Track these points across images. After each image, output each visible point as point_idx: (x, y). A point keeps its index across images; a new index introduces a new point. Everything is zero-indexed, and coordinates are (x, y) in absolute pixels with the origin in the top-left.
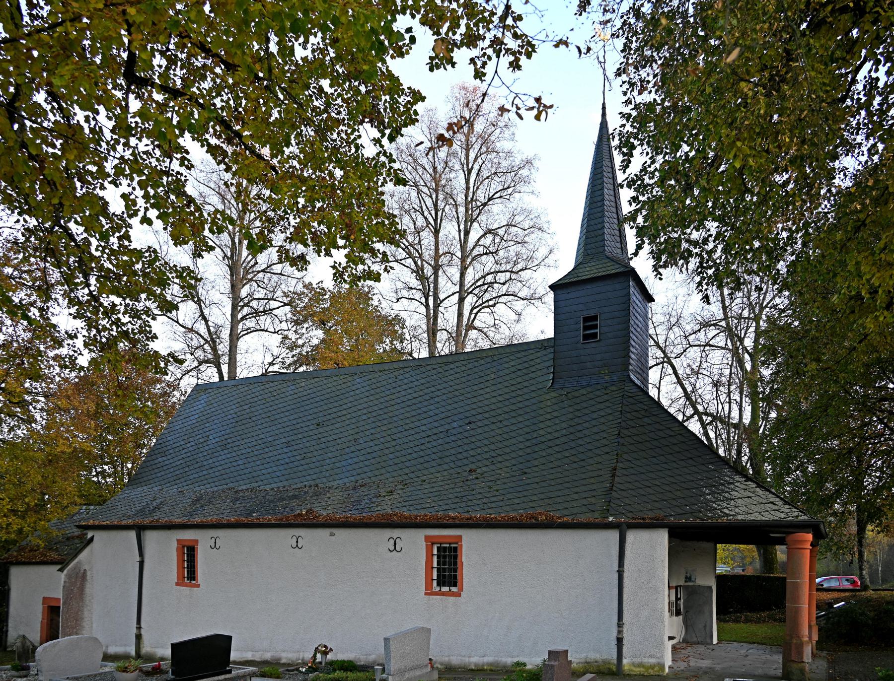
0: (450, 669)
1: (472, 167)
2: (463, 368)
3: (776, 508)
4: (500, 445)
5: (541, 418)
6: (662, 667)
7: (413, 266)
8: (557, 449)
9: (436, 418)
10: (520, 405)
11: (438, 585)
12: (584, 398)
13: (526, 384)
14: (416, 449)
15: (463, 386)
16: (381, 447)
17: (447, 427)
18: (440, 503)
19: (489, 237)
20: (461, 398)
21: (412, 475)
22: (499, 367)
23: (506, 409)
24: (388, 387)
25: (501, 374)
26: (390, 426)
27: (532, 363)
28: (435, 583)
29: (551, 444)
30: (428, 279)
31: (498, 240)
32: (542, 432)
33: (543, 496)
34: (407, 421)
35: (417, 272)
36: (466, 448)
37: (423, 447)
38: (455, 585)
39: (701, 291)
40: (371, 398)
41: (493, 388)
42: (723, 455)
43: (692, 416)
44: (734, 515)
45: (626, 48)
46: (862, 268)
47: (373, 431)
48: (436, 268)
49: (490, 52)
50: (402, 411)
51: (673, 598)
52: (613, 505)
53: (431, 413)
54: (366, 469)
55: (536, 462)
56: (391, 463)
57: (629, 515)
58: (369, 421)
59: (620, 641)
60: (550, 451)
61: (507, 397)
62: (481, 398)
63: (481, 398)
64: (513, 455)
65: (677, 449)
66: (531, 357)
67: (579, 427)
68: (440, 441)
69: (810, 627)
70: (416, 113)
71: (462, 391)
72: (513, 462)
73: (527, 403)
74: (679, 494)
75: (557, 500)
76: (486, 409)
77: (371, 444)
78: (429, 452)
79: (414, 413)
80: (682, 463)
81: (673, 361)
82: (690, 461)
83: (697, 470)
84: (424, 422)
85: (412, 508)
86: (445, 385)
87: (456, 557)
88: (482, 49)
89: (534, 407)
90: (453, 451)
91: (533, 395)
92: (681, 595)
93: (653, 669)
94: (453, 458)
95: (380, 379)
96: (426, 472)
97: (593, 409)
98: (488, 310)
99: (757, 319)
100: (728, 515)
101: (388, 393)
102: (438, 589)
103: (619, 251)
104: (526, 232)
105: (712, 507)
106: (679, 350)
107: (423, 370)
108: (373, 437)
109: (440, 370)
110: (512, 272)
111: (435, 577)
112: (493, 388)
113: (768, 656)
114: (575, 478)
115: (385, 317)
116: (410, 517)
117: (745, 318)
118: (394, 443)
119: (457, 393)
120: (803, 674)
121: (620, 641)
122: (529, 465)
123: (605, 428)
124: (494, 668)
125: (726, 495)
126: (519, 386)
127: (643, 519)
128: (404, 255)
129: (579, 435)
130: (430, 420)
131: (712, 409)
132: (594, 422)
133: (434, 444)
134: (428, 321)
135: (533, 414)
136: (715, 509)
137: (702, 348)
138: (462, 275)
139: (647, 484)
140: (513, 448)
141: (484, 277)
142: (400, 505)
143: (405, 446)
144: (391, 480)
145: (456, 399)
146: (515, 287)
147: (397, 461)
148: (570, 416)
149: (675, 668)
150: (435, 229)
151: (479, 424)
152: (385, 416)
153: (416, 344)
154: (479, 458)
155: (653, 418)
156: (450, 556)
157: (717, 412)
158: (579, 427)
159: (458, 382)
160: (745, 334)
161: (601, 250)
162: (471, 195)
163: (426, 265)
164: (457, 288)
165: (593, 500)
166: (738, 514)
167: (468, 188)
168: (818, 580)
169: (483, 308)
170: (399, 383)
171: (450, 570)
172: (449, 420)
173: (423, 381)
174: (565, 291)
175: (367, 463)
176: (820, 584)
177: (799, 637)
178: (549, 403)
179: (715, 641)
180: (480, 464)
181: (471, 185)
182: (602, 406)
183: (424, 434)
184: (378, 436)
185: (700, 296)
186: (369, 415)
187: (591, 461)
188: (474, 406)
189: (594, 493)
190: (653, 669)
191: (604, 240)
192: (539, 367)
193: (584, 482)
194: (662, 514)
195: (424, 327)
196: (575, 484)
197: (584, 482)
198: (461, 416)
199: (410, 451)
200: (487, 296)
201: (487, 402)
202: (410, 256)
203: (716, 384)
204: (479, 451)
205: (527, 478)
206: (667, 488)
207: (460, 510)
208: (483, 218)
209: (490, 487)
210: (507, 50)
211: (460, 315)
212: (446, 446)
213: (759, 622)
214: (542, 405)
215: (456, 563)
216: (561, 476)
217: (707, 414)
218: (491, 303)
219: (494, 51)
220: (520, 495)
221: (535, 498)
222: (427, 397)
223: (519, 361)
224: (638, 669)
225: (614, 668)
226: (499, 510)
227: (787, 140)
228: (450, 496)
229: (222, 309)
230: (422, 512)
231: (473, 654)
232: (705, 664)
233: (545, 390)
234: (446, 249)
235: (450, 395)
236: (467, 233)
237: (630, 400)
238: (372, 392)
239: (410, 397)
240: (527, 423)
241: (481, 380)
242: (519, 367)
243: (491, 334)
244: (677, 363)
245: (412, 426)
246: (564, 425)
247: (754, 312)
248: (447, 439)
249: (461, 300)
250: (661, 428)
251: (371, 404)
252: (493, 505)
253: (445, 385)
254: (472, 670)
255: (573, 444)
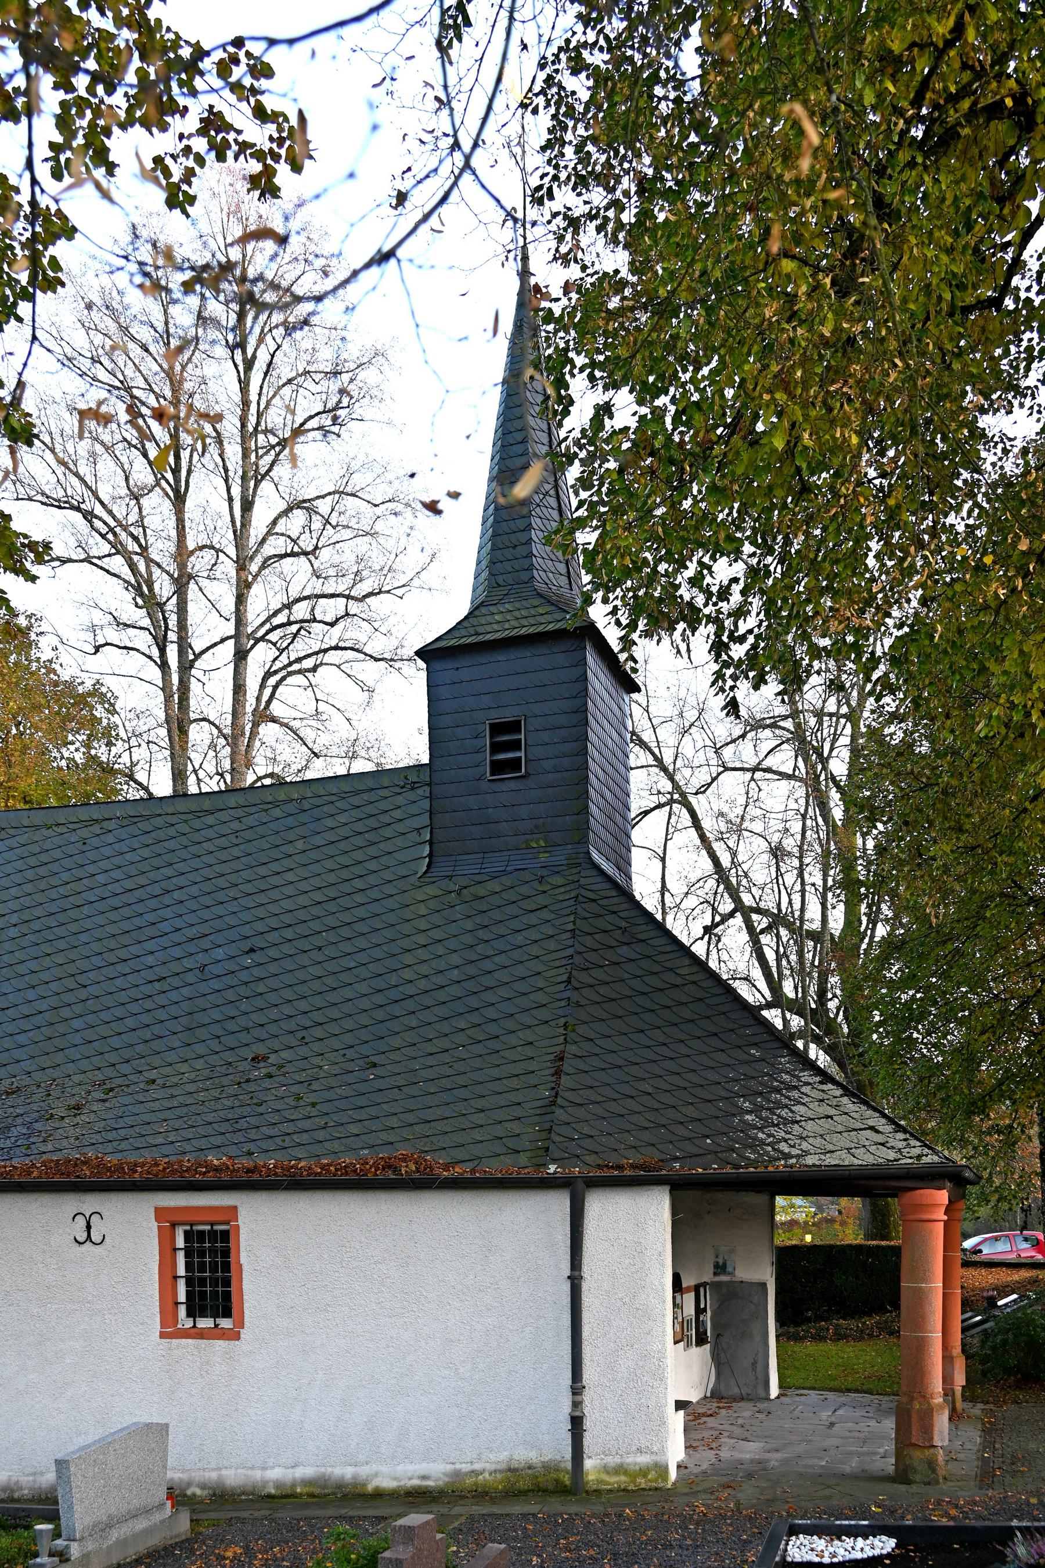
0: (222, 1496)
1: (254, 357)
2: (236, 825)
3: (880, 1138)
4: (318, 1001)
5: (406, 943)
6: (663, 1470)
7: (126, 572)
8: (442, 1011)
9: (176, 937)
10: (361, 912)
11: (190, 1314)
12: (496, 900)
13: (372, 865)
14: (134, 1008)
15: (236, 865)
16: (54, 1002)
17: (202, 959)
18: (189, 1134)
19: (299, 517)
20: (232, 893)
21: (125, 1069)
22: (314, 826)
23: (331, 921)
24: (67, 863)
25: (318, 840)
26: (73, 955)
27: (386, 819)
28: (182, 1311)
29: (427, 1000)
30: (161, 606)
31: (317, 524)
32: (408, 974)
33: (410, 1118)
34: (113, 944)
35: (138, 590)
36: (244, 1006)
37: (148, 1004)
38: (227, 1313)
39: (722, 690)
40: (28, 888)
41: (303, 872)
42: (791, 995)
43: (731, 915)
44: (798, 1156)
45: (553, 143)
46: (1032, 666)
47: (33, 965)
48: (182, 582)
49: (200, 145)
50: (100, 920)
51: (689, 1310)
52: (558, 1139)
53: (166, 927)
54: (20, 1054)
55: (396, 1042)
56: (77, 1039)
57: (590, 1159)
58: (25, 942)
59: (577, 1423)
60: (426, 1016)
61: (332, 892)
62: (275, 894)
63: (275, 894)
64: (349, 1024)
65: (687, 1014)
66: (383, 805)
67: (487, 965)
68: (186, 991)
69: (948, 1359)
70: (54, 263)
71: (233, 878)
72: (348, 1039)
73: (375, 908)
74: (691, 1111)
75: (440, 1126)
76: (288, 919)
77: (31, 995)
78: (162, 1015)
79: (126, 926)
80: (696, 1044)
81: (692, 799)
82: (714, 1041)
83: (728, 1061)
84: (150, 946)
85: (124, 1145)
86: (196, 863)
87: (226, 1253)
88: (181, 137)
89: (391, 918)
90: (216, 1014)
91: (389, 890)
92: (708, 1302)
93: (645, 1476)
94: (216, 1029)
95: (48, 845)
96: (156, 1061)
97: (515, 924)
98: (299, 679)
99: (853, 717)
100: (788, 1156)
101: (65, 876)
102: (189, 1324)
103: (563, 581)
104: (378, 511)
105: (755, 1138)
106: (702, 777)
107: (144, 826)
108: (33, 979)
109: (184, 828)
110: (348, 597)
111: (182, 1297)
112: (303, 872)
113: (873, 1423)
114: (478, 1076)
115: (70, 685)
116: (119, 1168)
117: (831, 715)
118: (83, 994)
119: (222, 882)
120: (934, 1471)
121: (577, 1423)
122: (381, 1046)
123: (541, 968)
124: (317, 1491)
125: (784, 1113)
126: (358, 870)
127: (619, 1167)
128: (106, 548)
129: (487, 981)
130: (164, 941)
131: (769, 903)
132: (516, 955)
133: (174, 996)
134: (168, 699)
135: (389, 933)
136: (763, 1143)
137: (749, 775)
138: (241, 600)
139: (627, 1090)
140: (347, 1008)
141: (288, 606)
142: (96, 1138)
143: (108, 1001)
144: (76, 1078)
145: (221, 896)
146: (354, 632)
147: (90, 1034)
148: (468, 939)
149: (691, 1466)
150: (176, 491)
151: (273, 953)
152: (61, 932)
153: (140, 754)
154: (273, 1029)
155: (639, 948)
156: (213, 1252)
157: (779, 910)
158: (487, 965)
159: (224, 855)
160: (832, 749)
161: (525, 576)
162: (252, 419)
163: (156, 572)
164: (230, 629)
165: (515, 1127)
166: (807, 1153)
167: (246, 403)
168: (968, 1244)
169: (290, 674)
170: (92, 855)
171: (215, 1282)
172: (205, 943)
173: (146, 852)
174: (450, 664)
175: (21, 1039)
176: (975, 1251)
177: (925, 1397)
178: (422, 910)
179: (774, 1391)
180: (275, 1044)
181: (253, 397)
182: (533, 919)
183: (150, 975)
184: (45, 976)
185: (721, 700)
186: (24, 928)
187: (512, 1040)
188: (261, 912)
189: (517, 1112)
190: (645, 1476)
191: (531, 555)
192: (400, 827)
193: (497, 1086)
194: (658, 1156)
195: (162, 716)
196: (478, 1090)
197: (497, 1086)
198: (233, 934)
199: (119, 1012)
200: (300, 648)
201: (287, 904)
202: (119, 549)
203: (777, 853)
204: (274, 1014)
205: (377, 1077)
206: (668, 1099)
207: (233, 1151)
208: (282, 471)
209: (298, 1098)
210: (244, 146)
211: (239, 688)
212: (201, 1003)
213: (860, 1339)
214: (408, 914)
215: (227, 1267)
216: (450, 1072)
217: (758, 911)
218: (308, 663)
219: (212, 146)
220: (362, 1114)
221: (394, 1122)
222: (157, 891)
223: (357, 814)
224: (613, 1479)
225: (567, 1480)
226: (318, 1149)
227: (855, 440)
228: (210, 1118)
229: (438, 81)
230: (148, 1155)
231: (271, 1461)
232: (750, 1451)
233: (413, 879)
234: (203, 540)
235: (208, 887)
236: (247, 506)
237: (592, 907)
238: (30, 874)
239: (117, 888)
240: (377, 953)
241: (275, 854)
242: (359, 827)
243: (309, 734)
244: (699, 803)
245: (123, 954)
246: (455, 959)
247: (848, 704)
248: (203, 988)
249: (241, 656)
250: (656, 968)
251: (27, 901)
252: (305, 1138)
253: (196, 863)
254: (270, 1496)
255: (473, 1001)
